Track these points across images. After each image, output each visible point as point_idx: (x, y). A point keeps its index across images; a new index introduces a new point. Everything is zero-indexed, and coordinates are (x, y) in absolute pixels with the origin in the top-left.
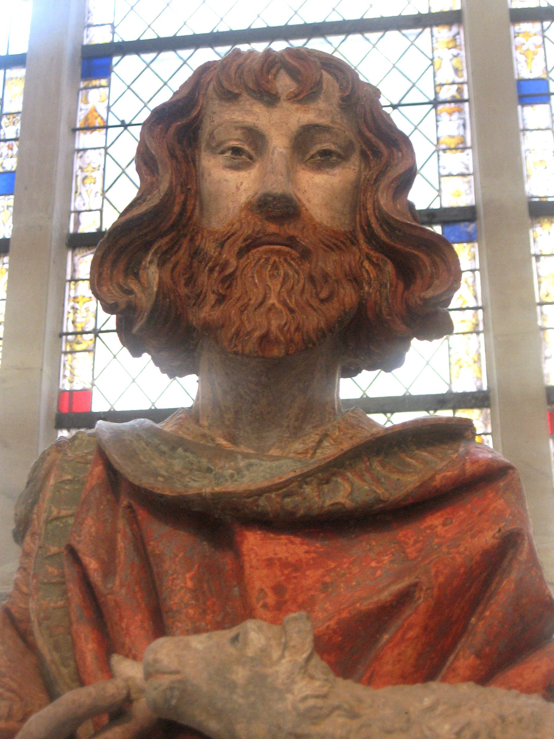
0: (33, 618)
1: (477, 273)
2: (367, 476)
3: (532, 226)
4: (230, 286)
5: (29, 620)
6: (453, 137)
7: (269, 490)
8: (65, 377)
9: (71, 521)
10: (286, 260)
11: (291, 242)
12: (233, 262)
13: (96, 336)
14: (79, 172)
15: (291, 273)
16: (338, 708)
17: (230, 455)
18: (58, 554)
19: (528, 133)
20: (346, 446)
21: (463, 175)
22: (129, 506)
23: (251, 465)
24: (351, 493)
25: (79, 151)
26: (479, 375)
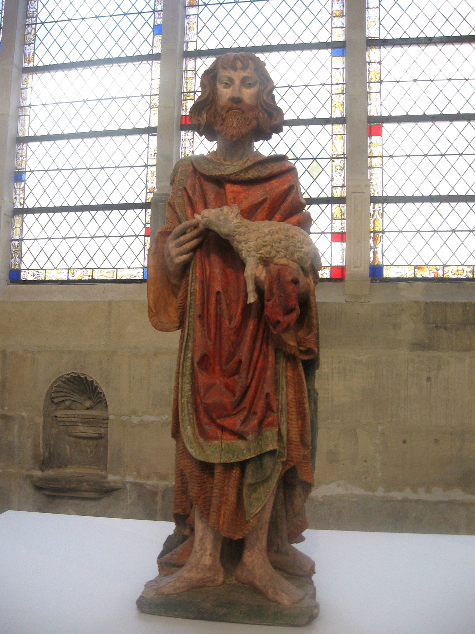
0: (176, 204)
1: (345, 69)
2: (257, 171)
3: (367, 50)
4: (224, 121)
5: (175, 205)
6: (338, 11)
7: (232, 174)
8: (183, 110)
9: (185, 180)
10: (238, 114)
11: (240, 109)
12: (225, 115)
13: (195, 93)
14: (187, 25)
15: (239, 117)
16: (243, 225)
17: (223, 165)
18: (181, 189)
19: (369, 10)
20: (254, 162)
21: (341, 27)
22: (199, 177)
23: (228, 167)
24: (253, 175)
25: (187, 16)
26: (343, 111)
